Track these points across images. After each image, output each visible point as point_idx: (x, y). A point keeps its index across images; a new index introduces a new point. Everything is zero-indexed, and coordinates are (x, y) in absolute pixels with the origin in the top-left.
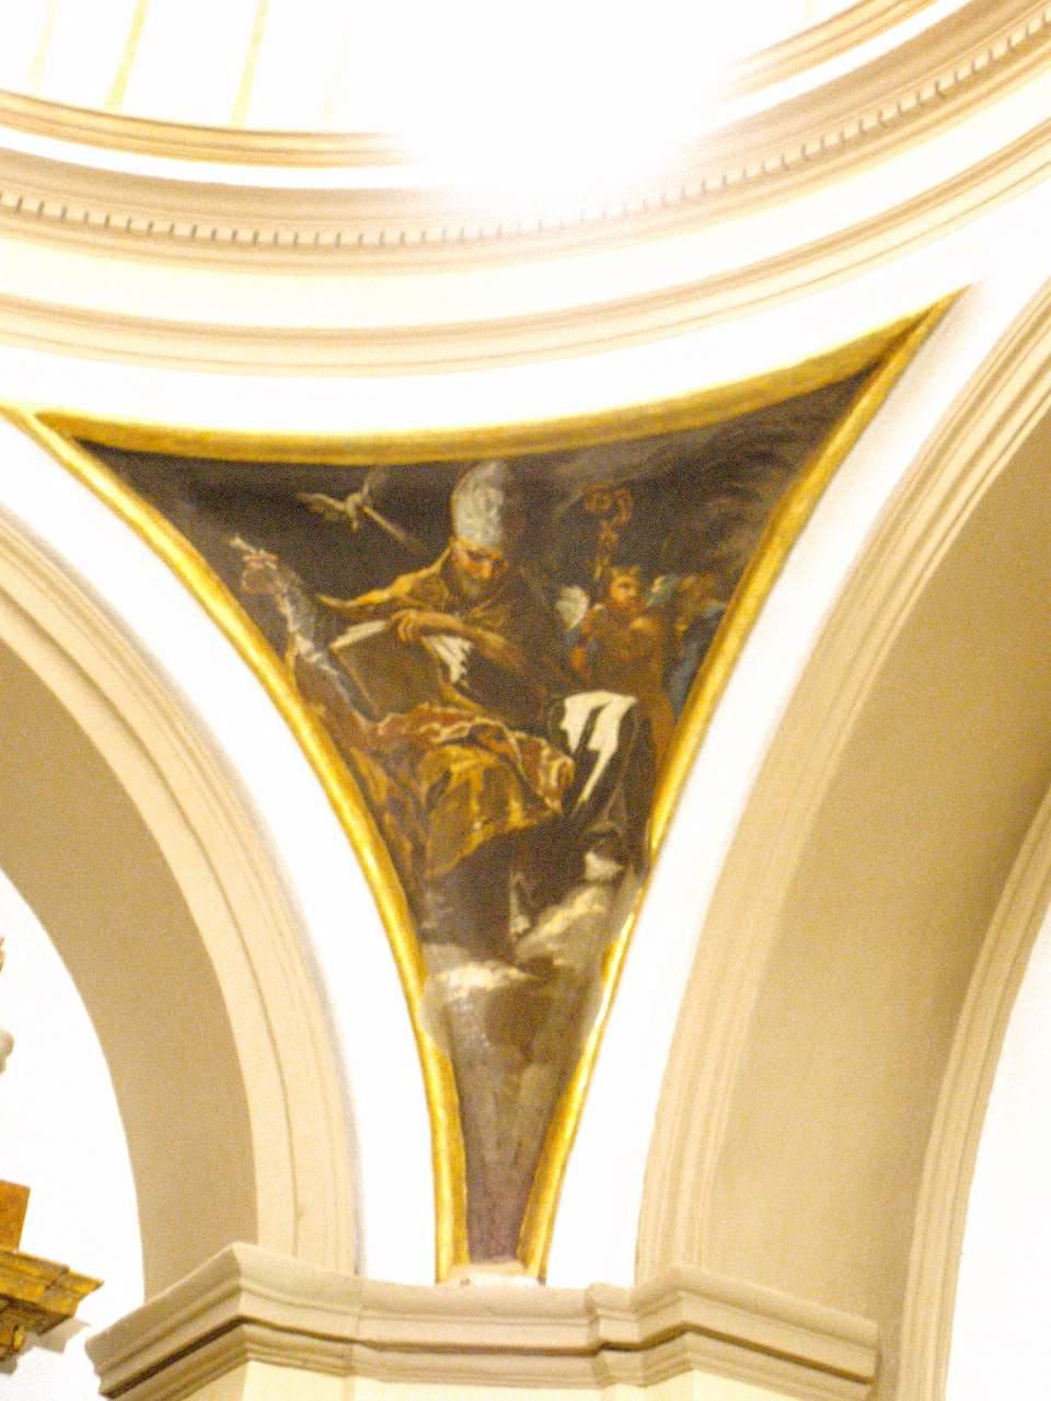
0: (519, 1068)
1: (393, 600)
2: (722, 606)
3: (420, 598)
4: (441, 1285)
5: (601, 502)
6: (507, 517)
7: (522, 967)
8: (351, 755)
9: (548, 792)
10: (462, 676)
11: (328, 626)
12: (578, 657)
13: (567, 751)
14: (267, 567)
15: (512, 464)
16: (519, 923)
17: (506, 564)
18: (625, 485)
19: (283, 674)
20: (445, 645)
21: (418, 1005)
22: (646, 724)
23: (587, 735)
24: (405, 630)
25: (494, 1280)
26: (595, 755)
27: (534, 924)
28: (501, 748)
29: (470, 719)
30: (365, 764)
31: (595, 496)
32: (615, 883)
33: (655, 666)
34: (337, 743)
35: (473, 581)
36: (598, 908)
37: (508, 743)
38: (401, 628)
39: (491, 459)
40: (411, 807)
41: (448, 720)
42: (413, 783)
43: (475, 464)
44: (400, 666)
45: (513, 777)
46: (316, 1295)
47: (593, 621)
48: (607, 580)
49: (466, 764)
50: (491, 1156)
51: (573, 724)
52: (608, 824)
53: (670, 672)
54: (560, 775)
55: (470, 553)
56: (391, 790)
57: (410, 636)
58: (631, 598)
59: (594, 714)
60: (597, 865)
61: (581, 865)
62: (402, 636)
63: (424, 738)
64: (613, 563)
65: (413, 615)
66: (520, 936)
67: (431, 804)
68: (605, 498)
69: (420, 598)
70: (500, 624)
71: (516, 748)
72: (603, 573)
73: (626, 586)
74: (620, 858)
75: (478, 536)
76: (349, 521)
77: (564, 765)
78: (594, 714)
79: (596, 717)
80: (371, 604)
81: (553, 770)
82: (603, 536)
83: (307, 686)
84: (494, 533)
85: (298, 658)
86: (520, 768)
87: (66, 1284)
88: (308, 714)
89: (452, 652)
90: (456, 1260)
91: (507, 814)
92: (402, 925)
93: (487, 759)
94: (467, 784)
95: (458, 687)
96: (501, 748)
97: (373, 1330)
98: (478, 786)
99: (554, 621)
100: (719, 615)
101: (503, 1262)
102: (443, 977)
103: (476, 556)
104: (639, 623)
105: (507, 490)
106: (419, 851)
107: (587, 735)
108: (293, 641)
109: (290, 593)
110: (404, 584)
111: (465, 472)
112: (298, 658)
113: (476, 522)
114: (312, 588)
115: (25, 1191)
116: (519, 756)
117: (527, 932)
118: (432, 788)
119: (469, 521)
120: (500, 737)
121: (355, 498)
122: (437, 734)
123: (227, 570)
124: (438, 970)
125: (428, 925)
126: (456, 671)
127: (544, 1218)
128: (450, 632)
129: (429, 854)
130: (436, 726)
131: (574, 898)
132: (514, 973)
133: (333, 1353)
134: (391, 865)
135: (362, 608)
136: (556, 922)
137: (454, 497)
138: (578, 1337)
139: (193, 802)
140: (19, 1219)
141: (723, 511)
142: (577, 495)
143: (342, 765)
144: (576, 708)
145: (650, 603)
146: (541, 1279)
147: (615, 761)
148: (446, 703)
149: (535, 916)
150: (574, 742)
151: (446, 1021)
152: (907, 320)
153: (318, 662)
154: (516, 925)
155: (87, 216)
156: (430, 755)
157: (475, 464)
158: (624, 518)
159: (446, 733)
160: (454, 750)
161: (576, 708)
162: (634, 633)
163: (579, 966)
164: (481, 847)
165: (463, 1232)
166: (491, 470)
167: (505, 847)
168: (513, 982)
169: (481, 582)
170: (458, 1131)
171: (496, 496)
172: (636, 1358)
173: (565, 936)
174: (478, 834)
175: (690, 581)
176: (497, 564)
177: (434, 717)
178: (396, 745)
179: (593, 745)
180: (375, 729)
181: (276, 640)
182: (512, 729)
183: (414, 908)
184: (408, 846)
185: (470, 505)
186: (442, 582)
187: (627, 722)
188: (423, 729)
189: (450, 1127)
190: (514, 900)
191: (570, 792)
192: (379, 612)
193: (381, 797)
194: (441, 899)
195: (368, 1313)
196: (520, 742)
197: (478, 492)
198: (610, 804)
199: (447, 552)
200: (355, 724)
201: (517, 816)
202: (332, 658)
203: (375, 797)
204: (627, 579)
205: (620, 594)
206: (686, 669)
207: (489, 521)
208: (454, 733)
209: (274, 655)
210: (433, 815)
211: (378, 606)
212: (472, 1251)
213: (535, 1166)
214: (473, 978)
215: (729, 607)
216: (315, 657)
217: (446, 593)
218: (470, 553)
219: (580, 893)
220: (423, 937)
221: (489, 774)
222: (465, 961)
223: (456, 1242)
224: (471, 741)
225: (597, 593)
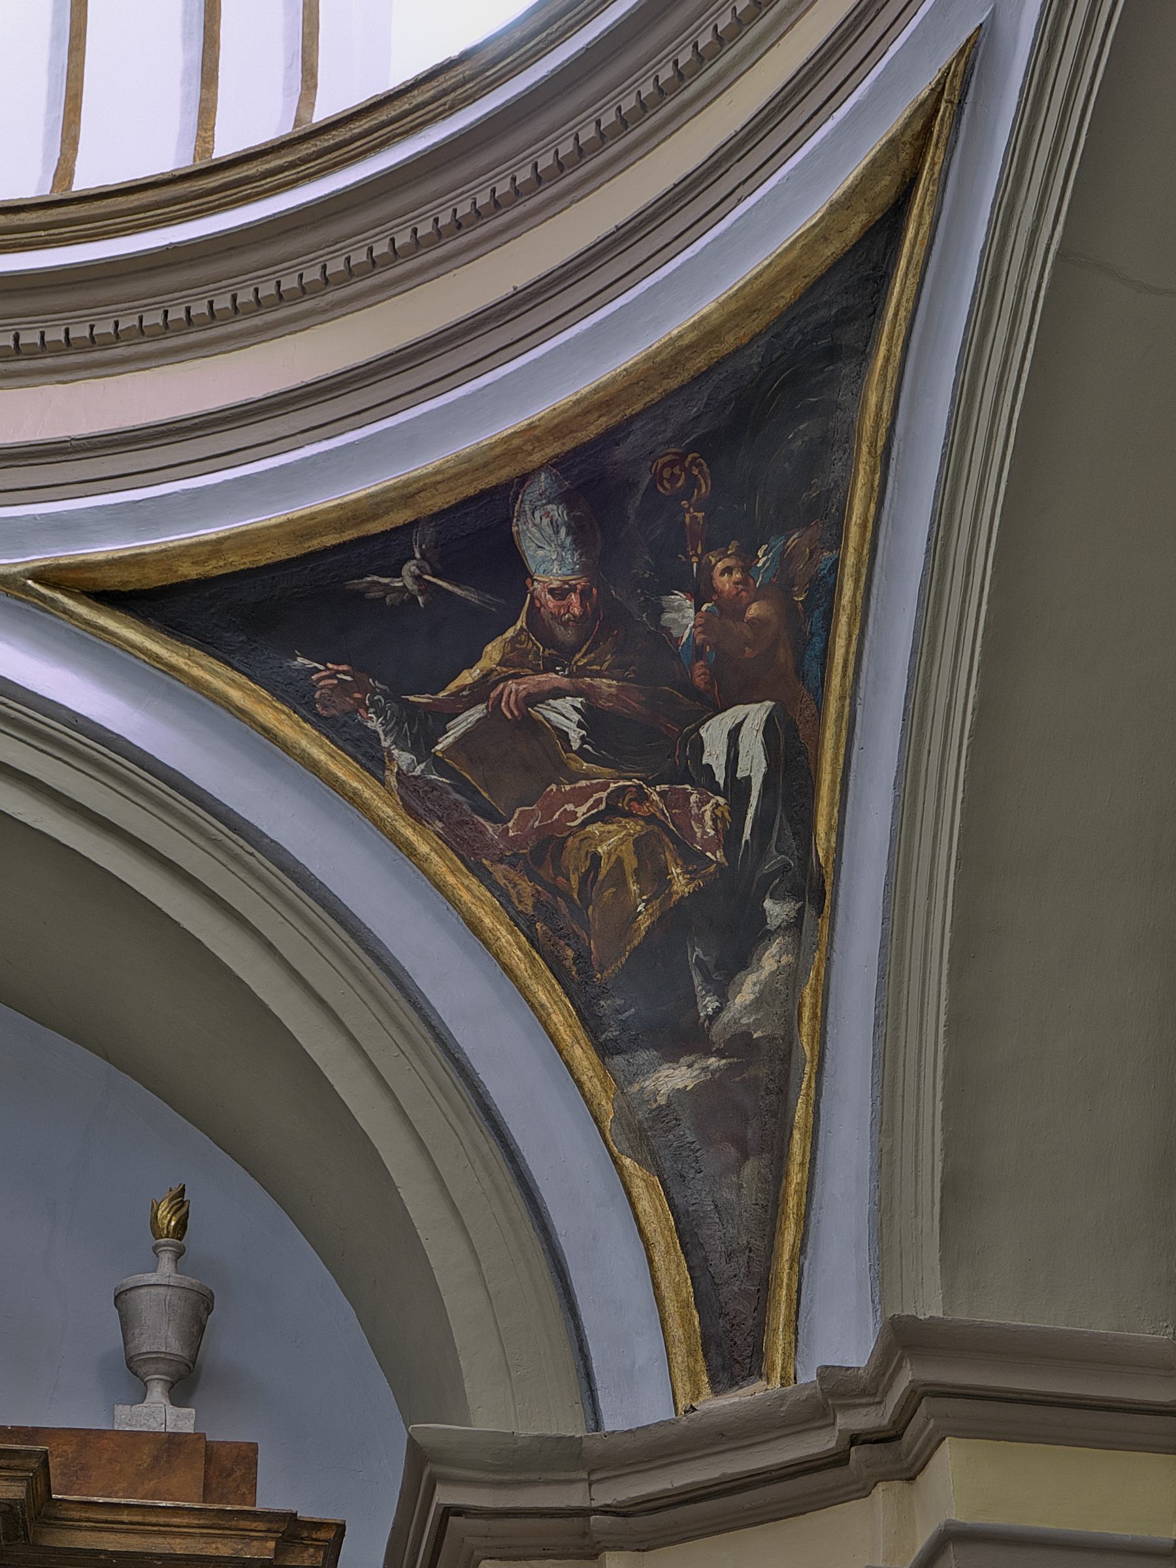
1: (486, 676)
3: (515, 663)
5: (674, 478)
6: (581, 534)
7: (720, 1054)
9: (708, 844)
10: (582, 738)
11: (420, 730)
12: (699, 674)
15: (559, 464)
16: (709, 1004)
18: (690, 449)
22: (792, 727)
27: (724, 999)
28: (645, 809)
29: (605, 787)
30: (499, 872)
31: (666, 474)
32: (795, 925)
33: (784, 655)
35: (565, 624)
41: (580, 797)
43: (524, 479)
44: (518, 740)
47: (705, 625)
50: (718, 1264)
51: (715, 756)
52: (777, 861)
55: (552, 591)
59: (734, 734)
64: (708, 549)
65: (512, 685)
66: (711, 1018)
67: (586, 901)
68: (677, 471)
70: (604, 668)
72: (699, 563)
73: (728, 570)
74: (796, 893)
78: (734, 734)
80: (464, 688)
81: (706, 815)
83: (417, 800)
89: (564, 714)
91: (670, 883)
93: (634, 827)
94: (620, 861)
95: (581, 752)
96: (645, 809)
98: (631, 863)
99: (663, 639)
103: (559, 593)
104: (753, 610)
105: (567, 499)
106: (581, 958)
108: (392, 759)
110: (493, 653)
111: (517, 494)
117: (718, 1011)
118: (583, 881)
119: (541, 552)
120: (642, 797)
121: (410, 567)
123: (297, 696)
126: (575, 736)
128: (558, 693)
132: (713, 1062)
136: (746, 992)
137: (515, 529)
141: (806, 439)
144: (714, 733)
148: (574, 777)
150: (720, 776)
154: (705, 1007)
157: (524, 479)
160: (595, 829)
161: (714, 733)
162: (752, 622)
164: (649, 930)
167: (676, 921)
171: (557, 511)
173: (758, 1003)
176: (584, 595)
181: (372, 760)
182: (652, 784)
191: (729, 836)
192: (480, 691)
196: (659, 793)
202: (438, 764)
204: (728, 562)
205: (724, 583)
207: (562, 547)
208: (589, 810)
211: (471, 686)
212: (713, 1381)
214: (675, 1078)
218: (552, 591)
225: (701, 592)
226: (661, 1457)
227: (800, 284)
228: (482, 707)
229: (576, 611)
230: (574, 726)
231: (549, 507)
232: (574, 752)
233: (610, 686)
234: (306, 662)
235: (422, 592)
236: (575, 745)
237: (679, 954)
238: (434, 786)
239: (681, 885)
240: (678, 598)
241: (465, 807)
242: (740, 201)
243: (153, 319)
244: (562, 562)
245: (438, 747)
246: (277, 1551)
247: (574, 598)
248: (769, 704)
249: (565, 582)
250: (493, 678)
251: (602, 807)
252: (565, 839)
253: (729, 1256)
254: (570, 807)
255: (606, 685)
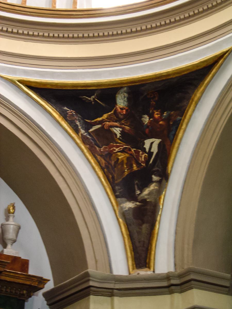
0: (141, 225)
1: (103, 120)
2: (181, 118)
3: (109, 119)
4: (131, 275)
6: (129, 100)
7: (139, 202)
8: (95, 156)
9: (142, 162)
10: (120, 136)
11: (87, 127)
12: (147, 131)
13: (146, 153)
14: (73, 114)
15: (129, 87)
16: (138, 192)
17: (129, 110)
19: (79, 138)
20: (115, 129)
21: (117, 212)
23: (150, 148)
24: (106, 126)
25: (143, 273)
26: (153, 153)
27: (141, 192)
28: (130, 152)
29: (122, 146)
30: (99, 157)
32: (160, 182)
34: (92, 153)
35: (121, 115)
36: (156, 188)
37: (132, 151)
38: (105, 126)
39: (125, 87)
40: (110, 166)
41: (117, 147)
42: (110, 162)
44: (105, 136)
45: (133, 159)
46: (104, 279)
47: (150, 122)
48: (153, 113)
49: (122, 156)
50: (137, 244)
51: (147, 146)
53: (169, 134)
54: (145, 158)
55: (120, 108)
56: (105, 163)
57: (107, 128)
58: (159, 117)
59: (152, 143)
60: (155, 178)
61: (152, 178)
62: (105, 128)
63: (112, 151)
64: (155, 109)
65: (107, 123)
69: (109, 119)
71: (134, 152)
74: (159, 176)
75: (122, 104)
76: (91, 102)
77: (145, 155)
78: (152, 143)
79: (152, 144)
81: (143, 157)
82: (152, 103)
83: (84, 140)
84: (126, 103)
85: (82, 134)
86: (135, 157)
87: (42, 281)
88: (86, 147)
89: (117, 131)
90: (133, 269)
91: (133, 167)
92: (112, 194)
93: (127, 155)
96: (130, 152)
97: (117, 286)
98: (125, 161)
99: (141, 123)
100: (181, 120)
101: (144, 268)
102: (122, 205)
103: (122, 109)
104: (161, 123)
105: (128, 93)
106: (113, 177)
107: (150, 148)
109: (79, 119)
110: (105, 116)
112: (82, 134)
113: (121, 102)
114: (83, 118)
115: (28, 260)
116: (135, 154)
117: (140, 194)
118: (115, 162)
119: (120, 101)
121: (93, 97)
122: (115, 150)
123: (64, 115)
124: (120, 204)
125: (118, 194)
126: (119, 135)
127: (152, 258)
128: (117, 127)
129: (115, 178)
130: (114, 148)
131: (150, 185)
132: (138, 203)
133: (110, 293)
134: (107, 180)
135: (96, 122)
136: (146, 192)
138: (165, 284)
139: (62, 170)
140: (27, 267)
142: (146, 94)
143: (94, 159)
145: (163, 118)
146: (154, 272)
147: (157, 154)
149: (142, 191)
150: (147, 150)
151: (124, 215)
152: (224, 52)
153: (86, 135)
155: (54, 35)
156: (114, 155)
157: (122, 88)
158: (156, 99)
159: (117, 150)
160: (119, 154)
161: (147, 143)
162: (161, 125)
163: (153, 201)
164: (127, 175)
165: (134, 263)
166: (125, 89)
167: (133, 175)
168: (138, 205)
169: (124, 114)
170: (130, 240)
171: (126, 95)
172: (179, 287)
173: (149, 194)
174: (126, 172)
175: (172, 113)
176: (127, 110)
177: (114, 146)
178: (107, 153)
179: (152, 151)
180: (101, 150)
181: (76, 131)
183: (114, 191)
184: (111, 176)
185: (120, 97)
186: (114, 115)
187: (159, 145)
188: (111, 149)
189: (128, 239)
190: (136, 187)
191: (147, 161)
192: (100, 122)
193: (103, 165)
194: (119, 188)
195: (117, 282)
196: (134, 150)
197: (122, 94)
198: (157, 164)
199: (115, 108)
200: (96, 148)
201: (135, 168)
202: (89, 134)
203: (102, 165)
205: (156, 116)
206: (173, 132)
207: (125, 101)
208: (119, 149)
209: (77, 135)
210: (115, 169)
213: (148, 247)
214: (129, 205)
215: (183, 118)
216: (85, 134)
217: (115, 117)
218: (120, 108)
219: (151, 184)
220: (116, 197)
221: (128, 159)
222: (126, 201)
223: (133, 265)
224: (123, 151)
225: (151, 116)
226: (131, 281)
227: (188, 72)
228: (100, 125)
229: (124, 113)
230: (118, 133)
231: (125, 94)
232: (118, 138)
233: (128, 128)
234: (67, 108)
235: (94, 102)
236: (118, 137)
237: (137, 182)
238: (88, 138)
239: (135, 168)
240: (146, 116)
241: (93, 143)
242: (179, 53)
243: (46, 34)
244: (124, 103)
245: (90, 131)
246: (38, 284)
247: (124, 110)
248: (160, 140)
249: (123, 107)
250: (104, 121)
251: (121, 150)
252: (112, 154)
253: (139, 242)
254: (114, 148)
255: (127, 128)
